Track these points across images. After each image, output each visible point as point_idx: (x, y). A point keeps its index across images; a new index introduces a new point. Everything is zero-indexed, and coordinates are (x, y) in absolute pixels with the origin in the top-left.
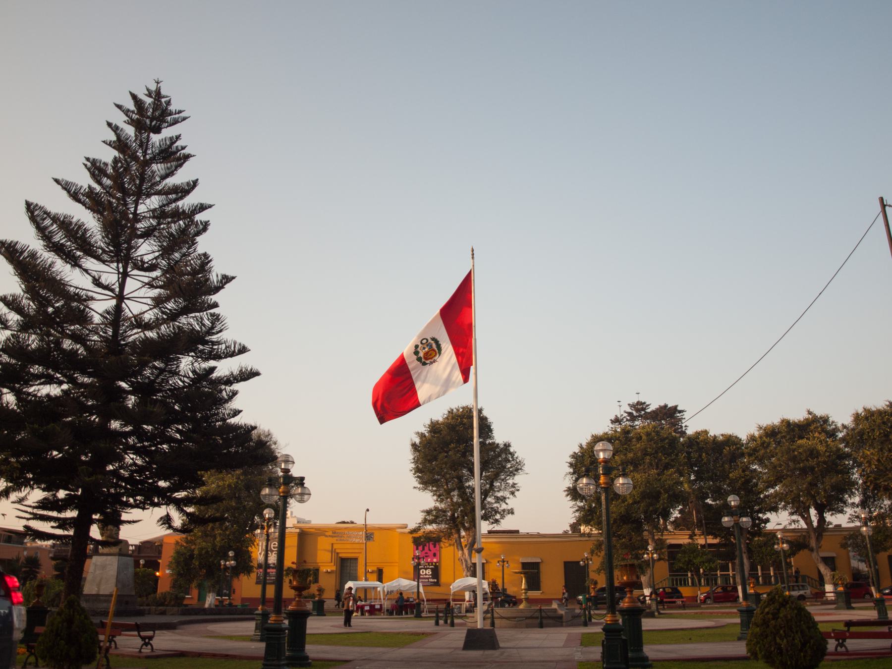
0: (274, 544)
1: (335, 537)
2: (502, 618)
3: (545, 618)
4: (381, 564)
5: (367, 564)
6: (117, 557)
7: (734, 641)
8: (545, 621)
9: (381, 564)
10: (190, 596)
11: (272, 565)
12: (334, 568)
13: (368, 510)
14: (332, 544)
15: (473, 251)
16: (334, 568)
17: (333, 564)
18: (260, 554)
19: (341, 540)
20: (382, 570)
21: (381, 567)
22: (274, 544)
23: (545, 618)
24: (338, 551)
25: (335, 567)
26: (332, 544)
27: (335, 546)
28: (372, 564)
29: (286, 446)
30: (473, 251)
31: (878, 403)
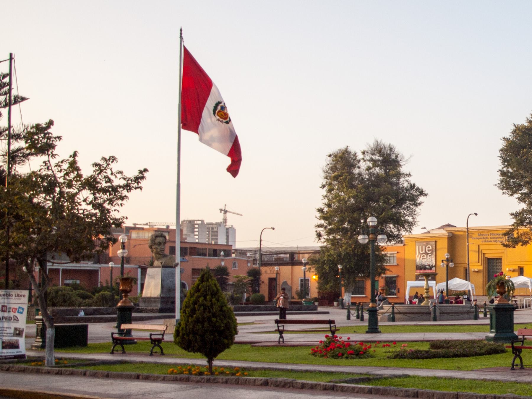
0: (429, 247)
1: (481, 238)
2: (400, 313)
3: (397, 313)
4: (522, 263)
5: (470, 264)
6: (161, 269)
7: (364, 333)
8: (397, 316)
9: (522, 263)
10: (396, 296)
11: (427, 267)
12: (481, 268)
13: (274, 229)
14: (479, 245)
15: (181, 30)
16: (481, 268)
17: (480, 264)
18: (418, 256)
19: (486, 241)
20: (523, 268)
21: (521, 266)
22: (429, 247)
23: (397, 313)
24: (484, 252)
25: (482, 267)
26: (479, 245)
27: (481, 248)
28: (513, 263)
29: (410, 158)
30: (181, 30)
31: (523, 122)
